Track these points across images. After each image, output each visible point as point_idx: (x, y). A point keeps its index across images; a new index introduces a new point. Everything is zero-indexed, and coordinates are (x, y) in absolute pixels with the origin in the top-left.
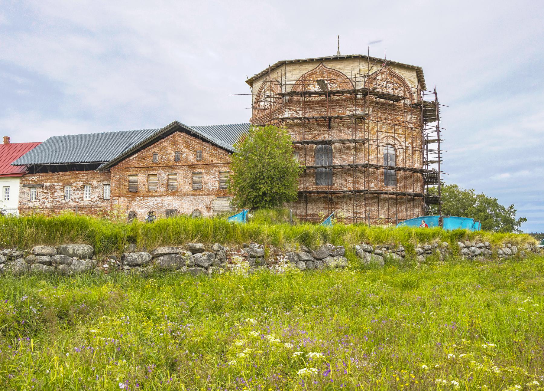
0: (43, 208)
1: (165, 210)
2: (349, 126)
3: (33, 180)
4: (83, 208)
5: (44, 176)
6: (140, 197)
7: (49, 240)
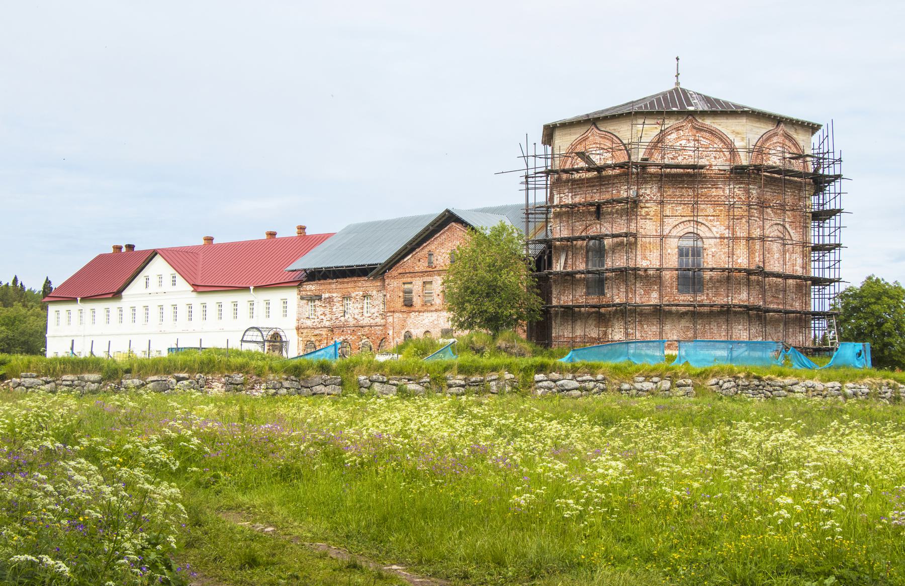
0: (322, 328)
1: (440, 329)
2: (620, 213)
3: (310, 290)
4: (362, 327)
5: (321, 284)
6: (415, 312)
7: (73, 372)
